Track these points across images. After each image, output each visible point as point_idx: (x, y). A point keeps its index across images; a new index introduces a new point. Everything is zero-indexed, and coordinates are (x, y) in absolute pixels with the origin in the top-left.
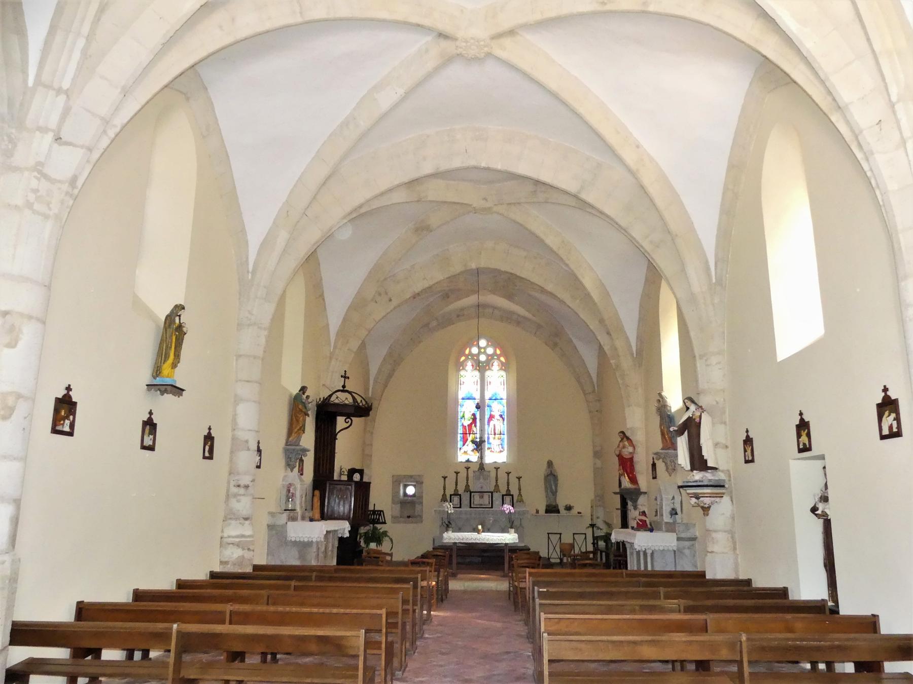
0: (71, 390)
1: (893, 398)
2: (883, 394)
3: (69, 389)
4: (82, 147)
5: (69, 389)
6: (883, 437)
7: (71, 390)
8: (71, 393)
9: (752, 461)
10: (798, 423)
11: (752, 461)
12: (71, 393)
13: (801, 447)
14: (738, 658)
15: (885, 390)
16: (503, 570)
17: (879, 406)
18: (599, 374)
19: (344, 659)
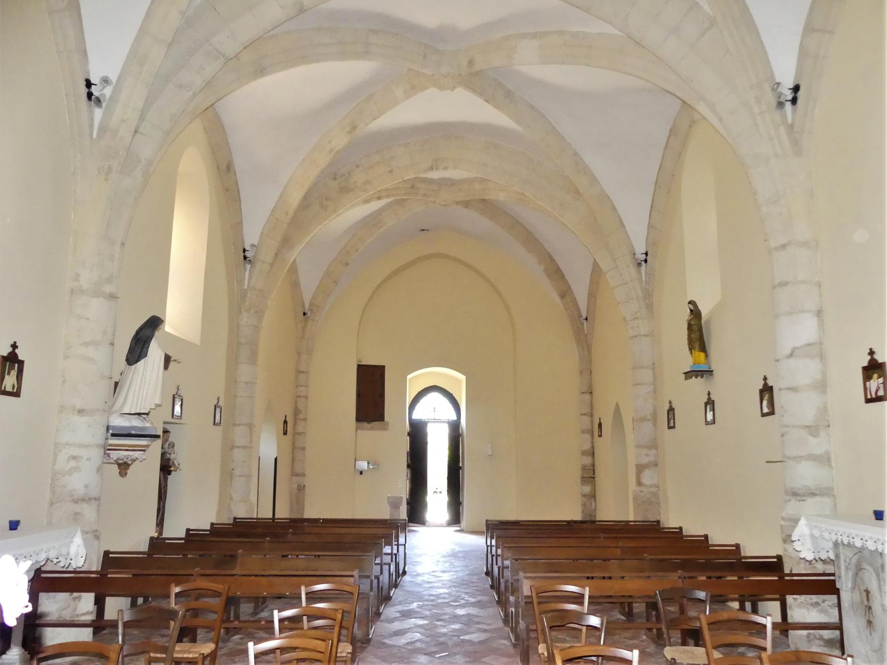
0: (17, 347)
1: (880, 361)
2: (869, 357)
3: (14, 346)
4: (244, 425)
5: (14, 346)
6: (868, 401)
7: (17, 347)
8: (17, 351)
9: (674, 427)
10: (761, 387)
11: (674, 427)
12: (17, 351)
13: (869, 397)
14: (834, 619)
15: (871, 353)
16: (834, 581)
17: (865, 369)
18: (592, 296)
19: (376, 602)
